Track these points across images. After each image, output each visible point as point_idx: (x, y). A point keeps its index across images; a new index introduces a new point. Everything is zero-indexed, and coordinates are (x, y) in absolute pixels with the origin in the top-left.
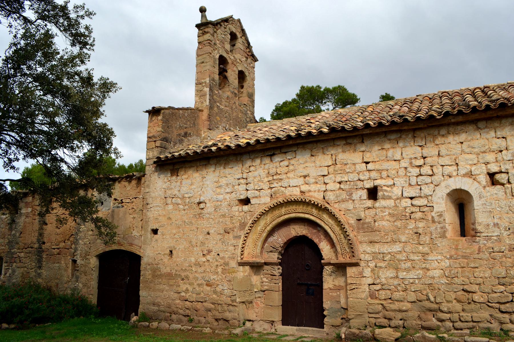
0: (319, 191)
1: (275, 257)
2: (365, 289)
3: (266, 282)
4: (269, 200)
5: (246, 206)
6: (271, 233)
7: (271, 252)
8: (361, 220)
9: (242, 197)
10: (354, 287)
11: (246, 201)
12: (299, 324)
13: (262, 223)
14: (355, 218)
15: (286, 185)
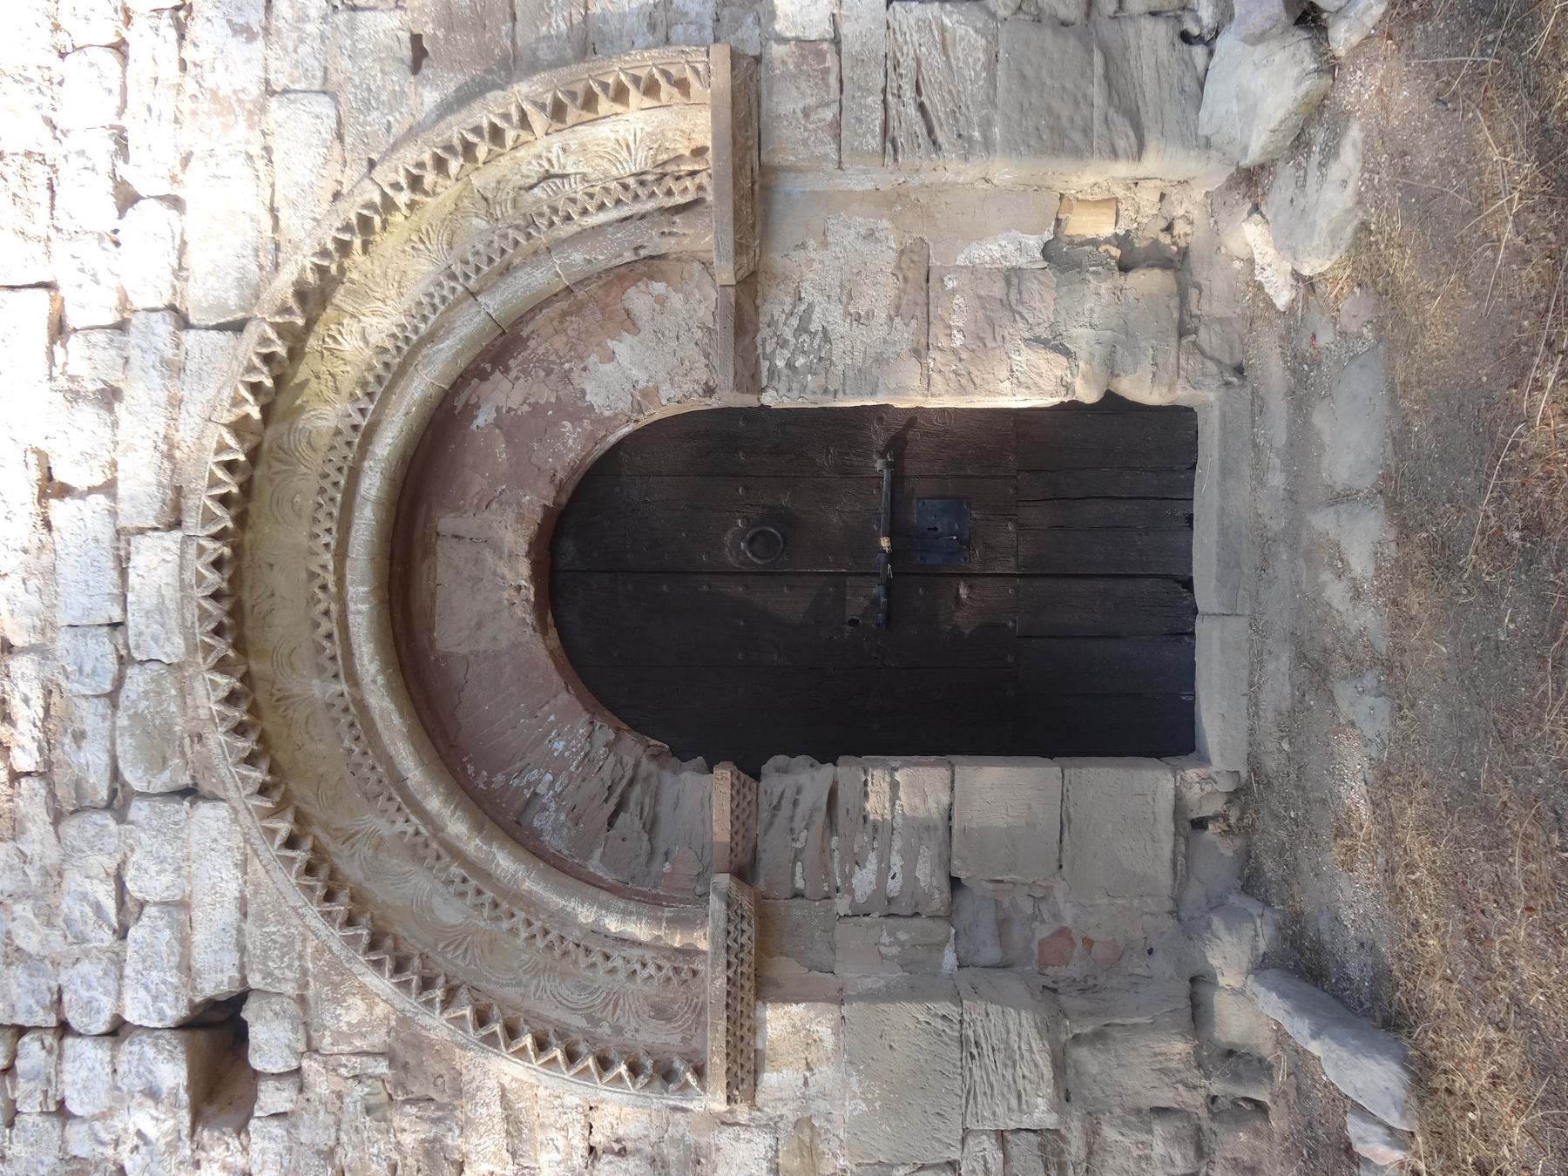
0: (174, 368)
1: (706, 798)
2: (924, 25)
3: (884, 860)
4: (222, 810)
5: (259, 1033)
6: (505, 818)
7: (651, 827)
8: (416, 39)
9: (173, 1073)
10: (912, 111)
11: (217, 1036)
12: (943, 410)
13: (410, 889)
14: (399, 78)
15: (101, 651)
